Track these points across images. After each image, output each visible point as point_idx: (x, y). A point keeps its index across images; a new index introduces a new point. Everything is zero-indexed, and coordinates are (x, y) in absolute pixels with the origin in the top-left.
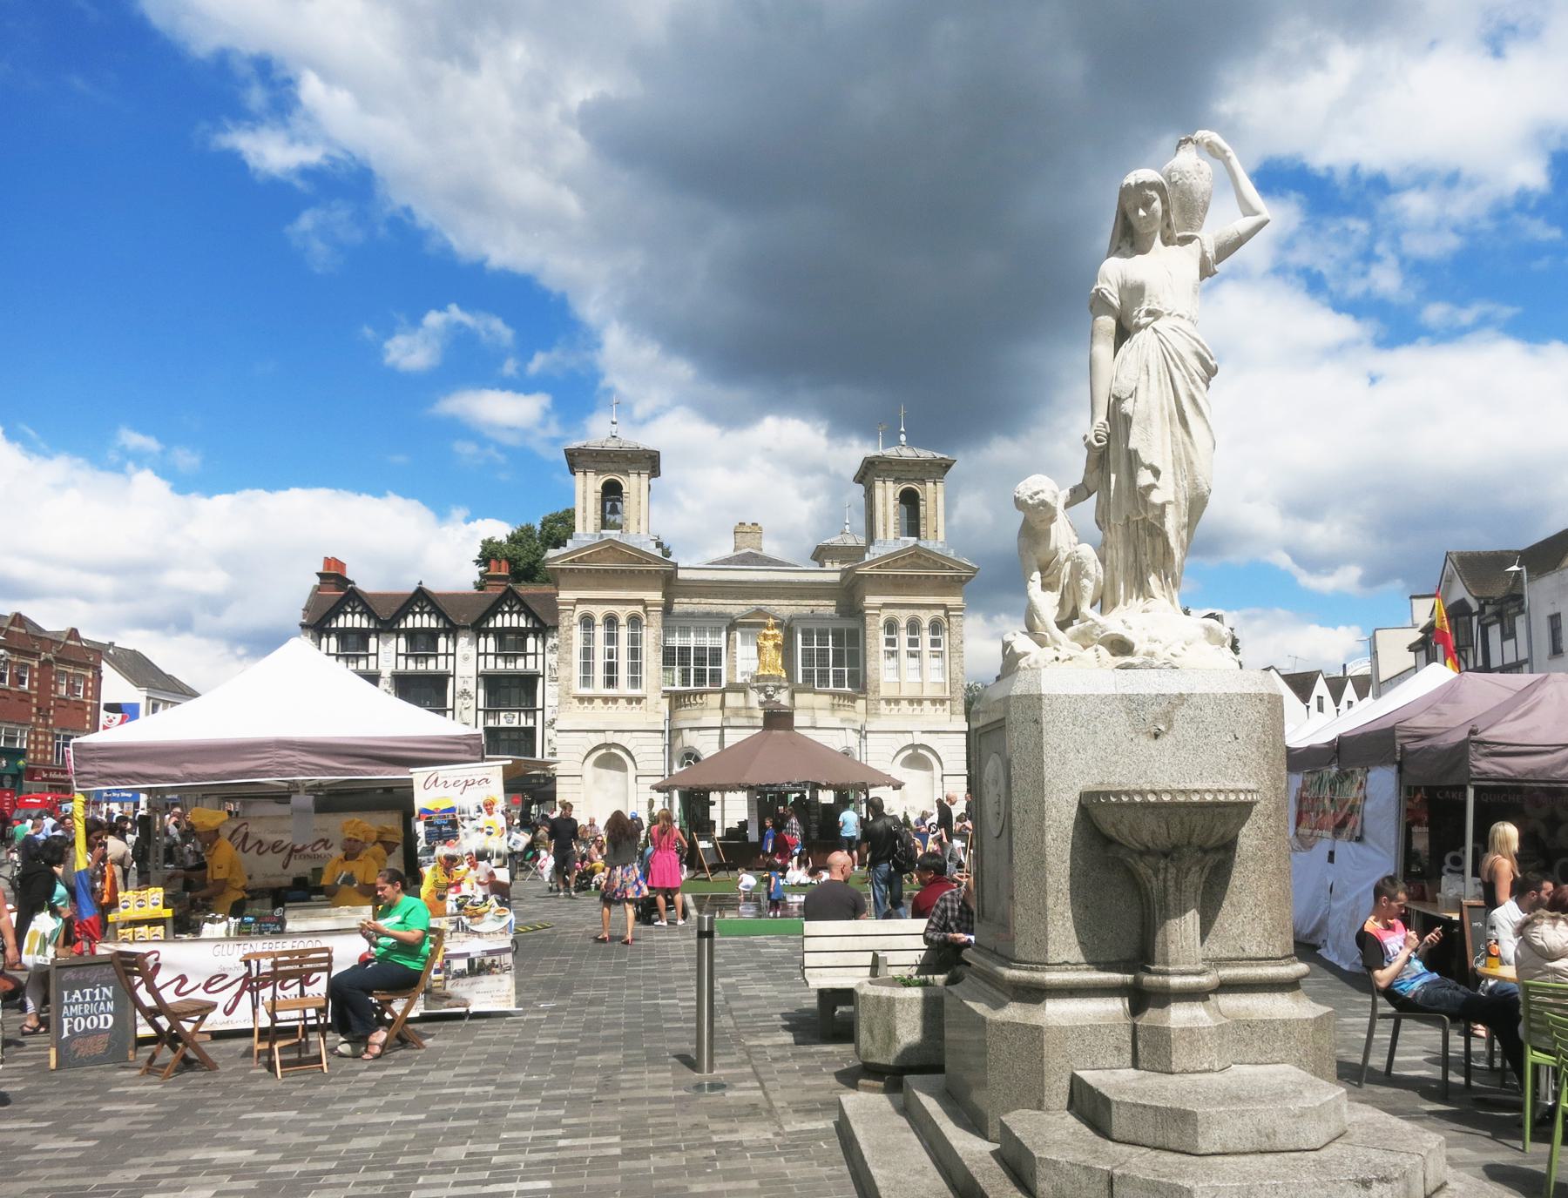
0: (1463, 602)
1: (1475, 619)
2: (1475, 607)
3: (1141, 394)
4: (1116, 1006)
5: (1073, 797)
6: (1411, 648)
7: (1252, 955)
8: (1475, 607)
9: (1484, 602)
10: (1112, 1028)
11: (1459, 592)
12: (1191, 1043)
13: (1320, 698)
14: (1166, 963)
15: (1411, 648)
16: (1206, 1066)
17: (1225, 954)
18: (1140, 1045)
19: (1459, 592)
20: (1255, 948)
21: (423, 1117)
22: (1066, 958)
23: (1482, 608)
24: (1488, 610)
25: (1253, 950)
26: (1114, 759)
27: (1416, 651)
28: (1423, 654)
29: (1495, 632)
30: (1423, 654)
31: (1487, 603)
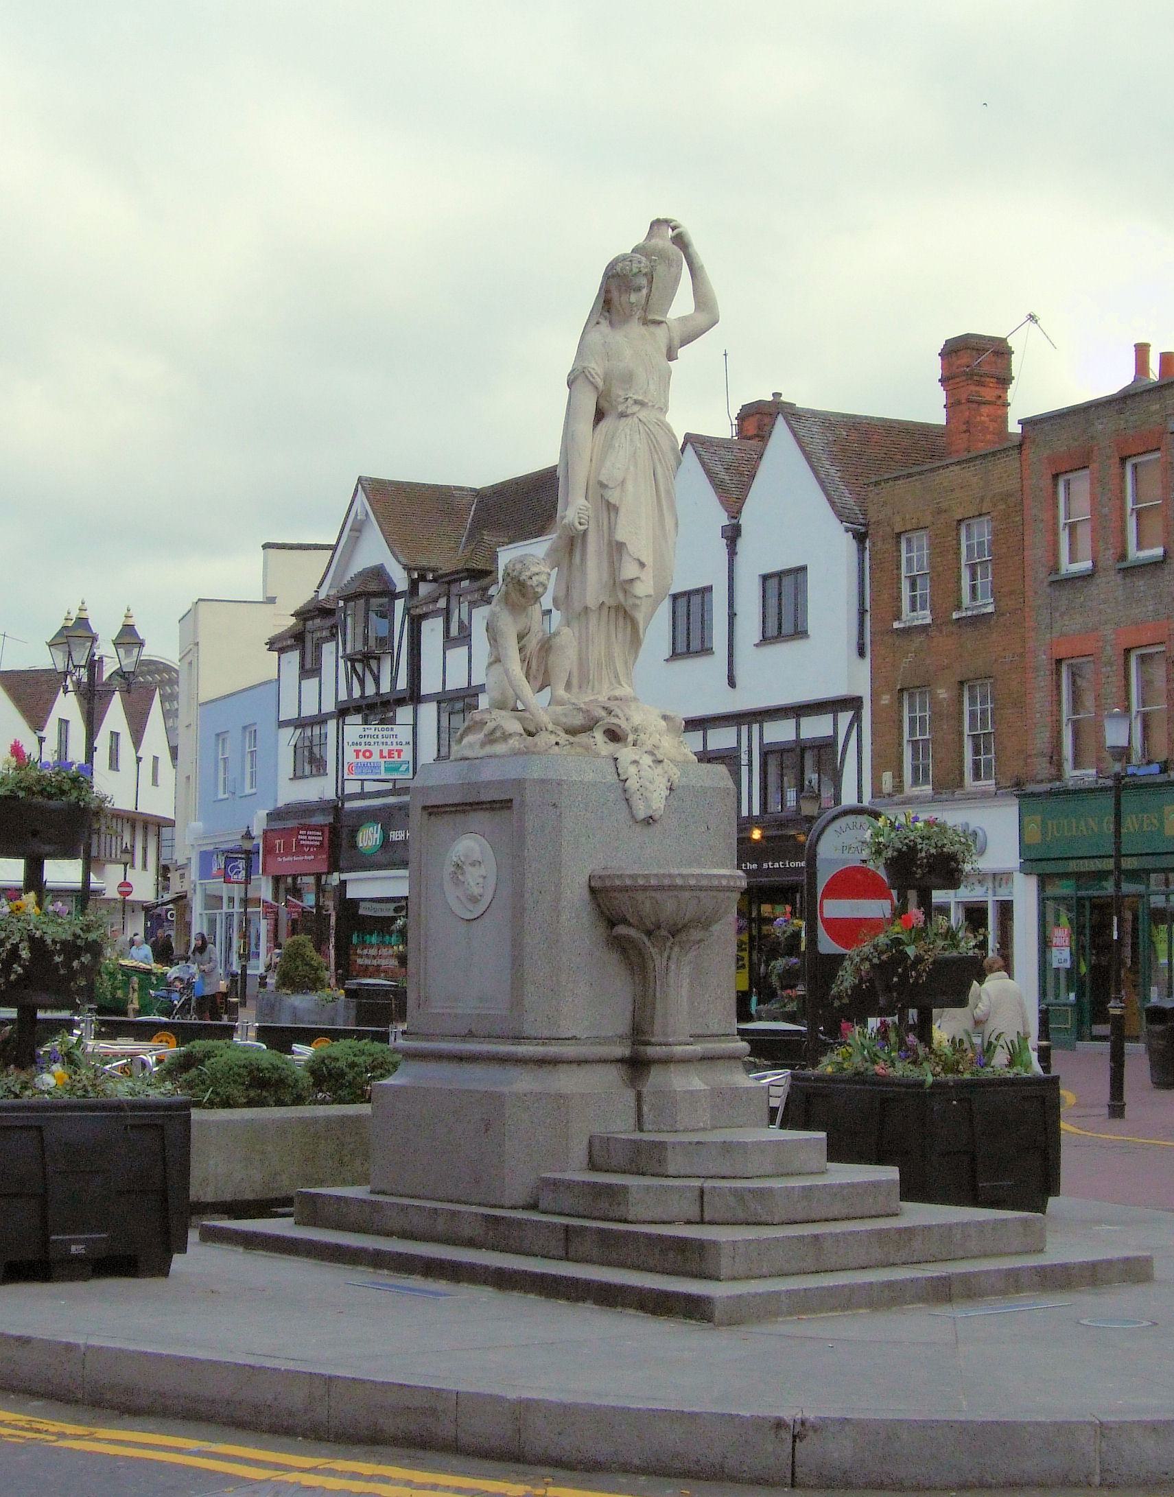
0: (378, 573)
1: (399, 605)
2: (401, 581)
3: (630, 486)
6: (272, 644)
7: (714, 1032)
8: (401, 581)
9: (418, 576)
11: (375, 552)
13: (64, 723)
14: (665, 1034)
15: (272, 644)
18: (645, 1109)
19: (375, 552)
21: (1115, 919)
23: (414, 585)
24: (424, 588)
25: (715, 1028)
27: (282, 651)
28: (294, 657)
29: (432, 631)
30: (294, 657)
31: (422, 578)
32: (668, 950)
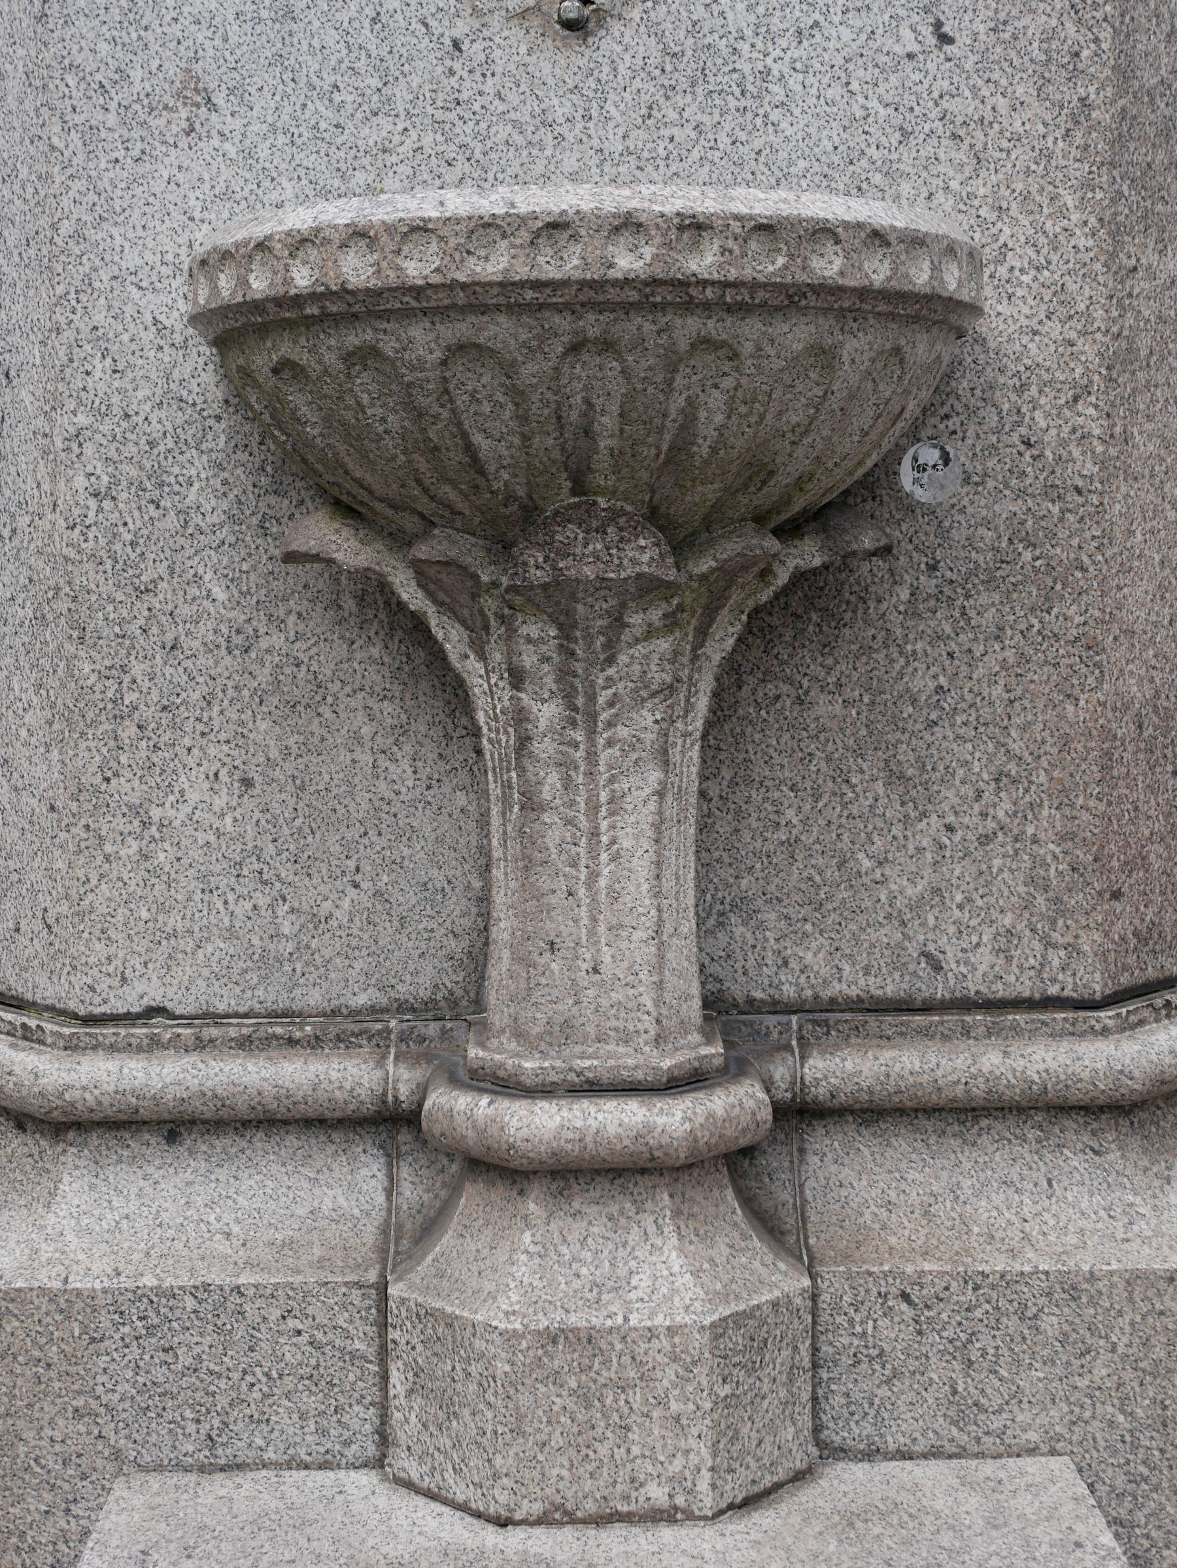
4: (351, 1191)
5: (174, 304)
7: (974, 986)
10: (293, 1303)
12: (584, 1398)
16: (657, 1494)
17: (851, 983)
20: (984, 959)
22: (145, 990)
25: (978, 969)
26: (371, 135)
32: (497, 630)
